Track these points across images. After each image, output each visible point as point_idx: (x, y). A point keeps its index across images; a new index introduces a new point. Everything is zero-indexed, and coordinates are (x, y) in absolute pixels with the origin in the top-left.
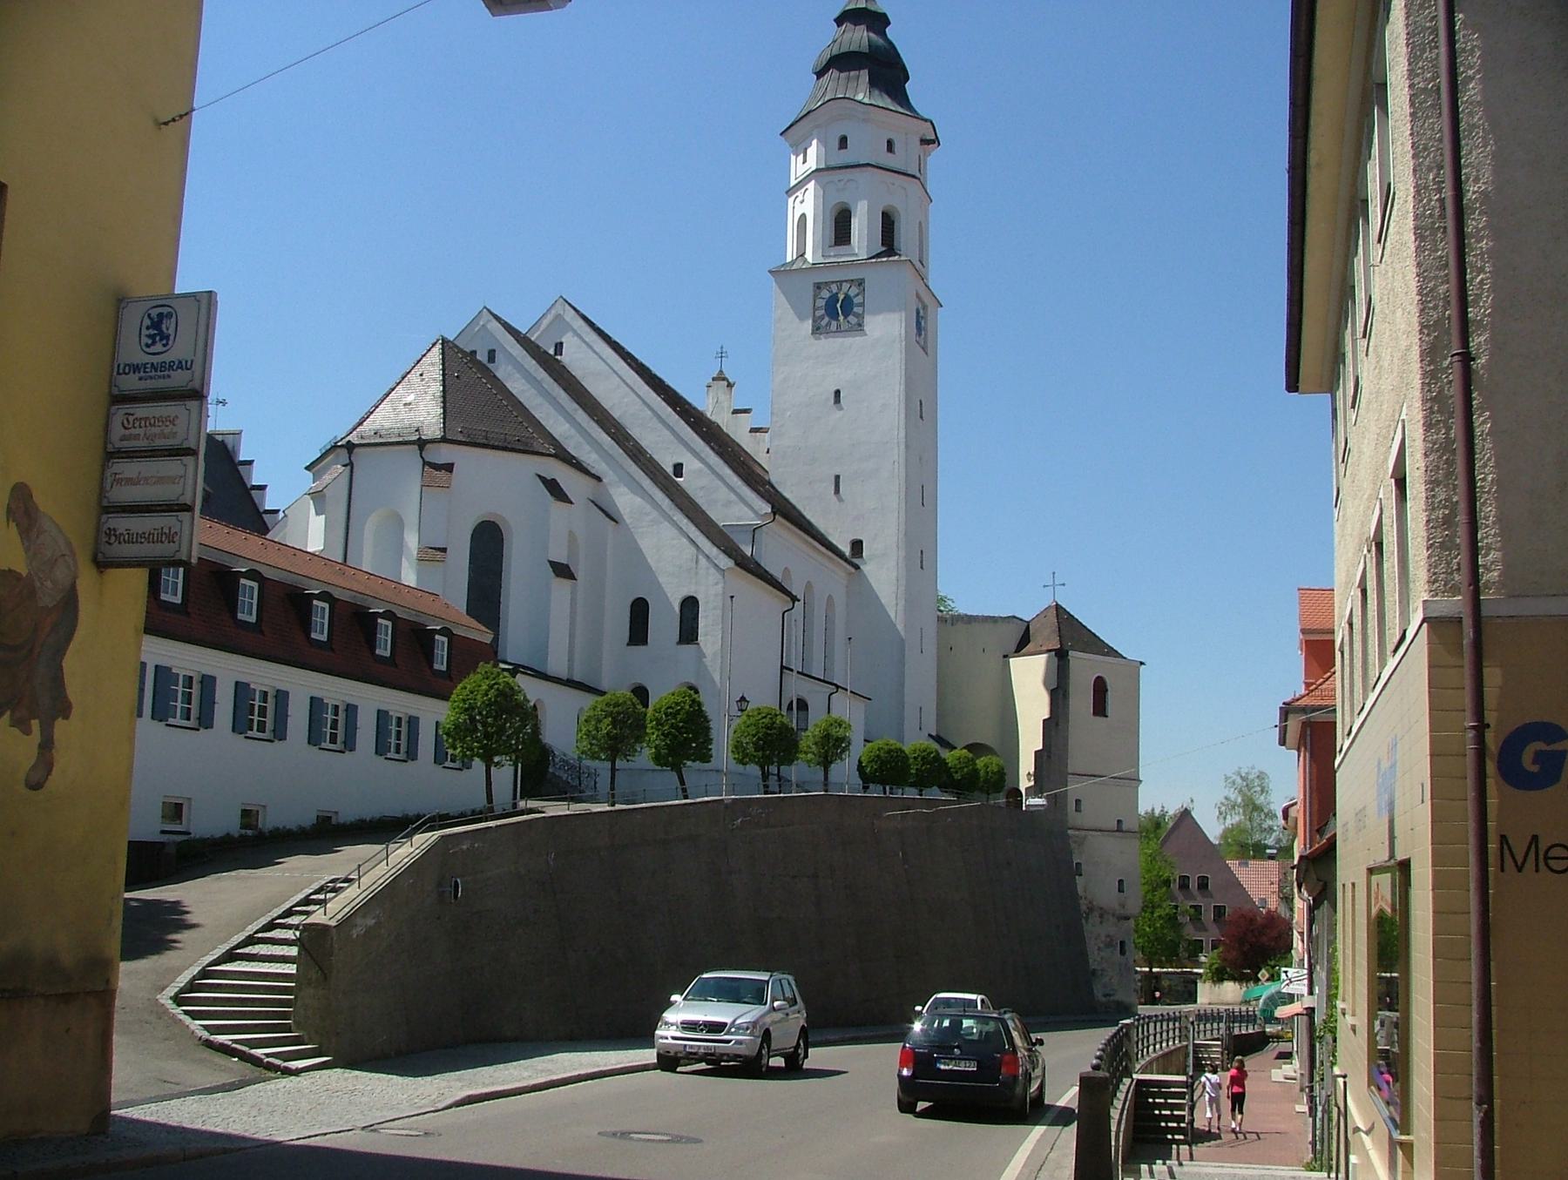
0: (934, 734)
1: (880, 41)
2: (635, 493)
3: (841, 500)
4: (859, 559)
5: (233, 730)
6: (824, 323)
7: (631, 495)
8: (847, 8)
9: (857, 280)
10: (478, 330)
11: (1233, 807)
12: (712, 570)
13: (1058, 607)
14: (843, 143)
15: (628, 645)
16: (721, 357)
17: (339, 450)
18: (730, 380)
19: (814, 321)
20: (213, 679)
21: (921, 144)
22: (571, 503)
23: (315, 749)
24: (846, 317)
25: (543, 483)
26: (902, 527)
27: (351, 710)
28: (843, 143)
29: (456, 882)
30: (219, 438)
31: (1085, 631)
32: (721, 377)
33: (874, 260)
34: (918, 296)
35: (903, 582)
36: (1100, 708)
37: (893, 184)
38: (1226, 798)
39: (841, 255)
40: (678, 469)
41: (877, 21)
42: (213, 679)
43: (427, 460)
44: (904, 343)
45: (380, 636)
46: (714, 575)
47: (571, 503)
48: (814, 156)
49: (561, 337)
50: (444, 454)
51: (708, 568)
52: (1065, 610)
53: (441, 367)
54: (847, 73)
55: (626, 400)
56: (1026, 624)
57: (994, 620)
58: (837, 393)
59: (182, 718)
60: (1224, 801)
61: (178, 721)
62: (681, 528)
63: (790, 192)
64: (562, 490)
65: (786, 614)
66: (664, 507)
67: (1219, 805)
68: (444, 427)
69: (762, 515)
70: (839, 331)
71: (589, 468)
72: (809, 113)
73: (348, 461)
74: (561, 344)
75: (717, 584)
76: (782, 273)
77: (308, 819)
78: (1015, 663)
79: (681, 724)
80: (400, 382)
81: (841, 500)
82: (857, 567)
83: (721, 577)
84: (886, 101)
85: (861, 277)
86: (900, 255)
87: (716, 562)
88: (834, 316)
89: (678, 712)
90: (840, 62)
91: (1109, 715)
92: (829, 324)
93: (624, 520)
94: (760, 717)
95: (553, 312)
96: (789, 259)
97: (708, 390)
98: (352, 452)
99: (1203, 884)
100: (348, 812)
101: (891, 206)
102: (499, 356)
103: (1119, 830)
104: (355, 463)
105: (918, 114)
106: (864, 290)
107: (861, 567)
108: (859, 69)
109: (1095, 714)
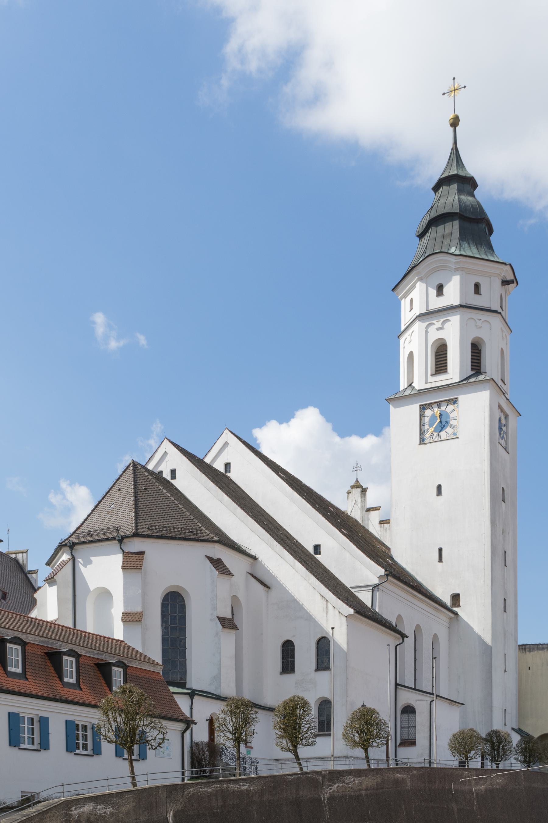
0: (516, 728)
8: (443, 176)
15: (281, 673)
16: (357, 470)
21: (502, 285)
23: (16, 750)
25: (208, 559)
30: (13, 556)
32: (357, 485)
34: (500, 407)
39: (441, 380)
40: (317, 548)
42: (47, 719)
53: (132, 483)
61: (26, 746)
65: (398, 647)
71: (247, 550)
96: (402, 388)
97: (348, 496)
101: (437, 285)
104: (75, 556)
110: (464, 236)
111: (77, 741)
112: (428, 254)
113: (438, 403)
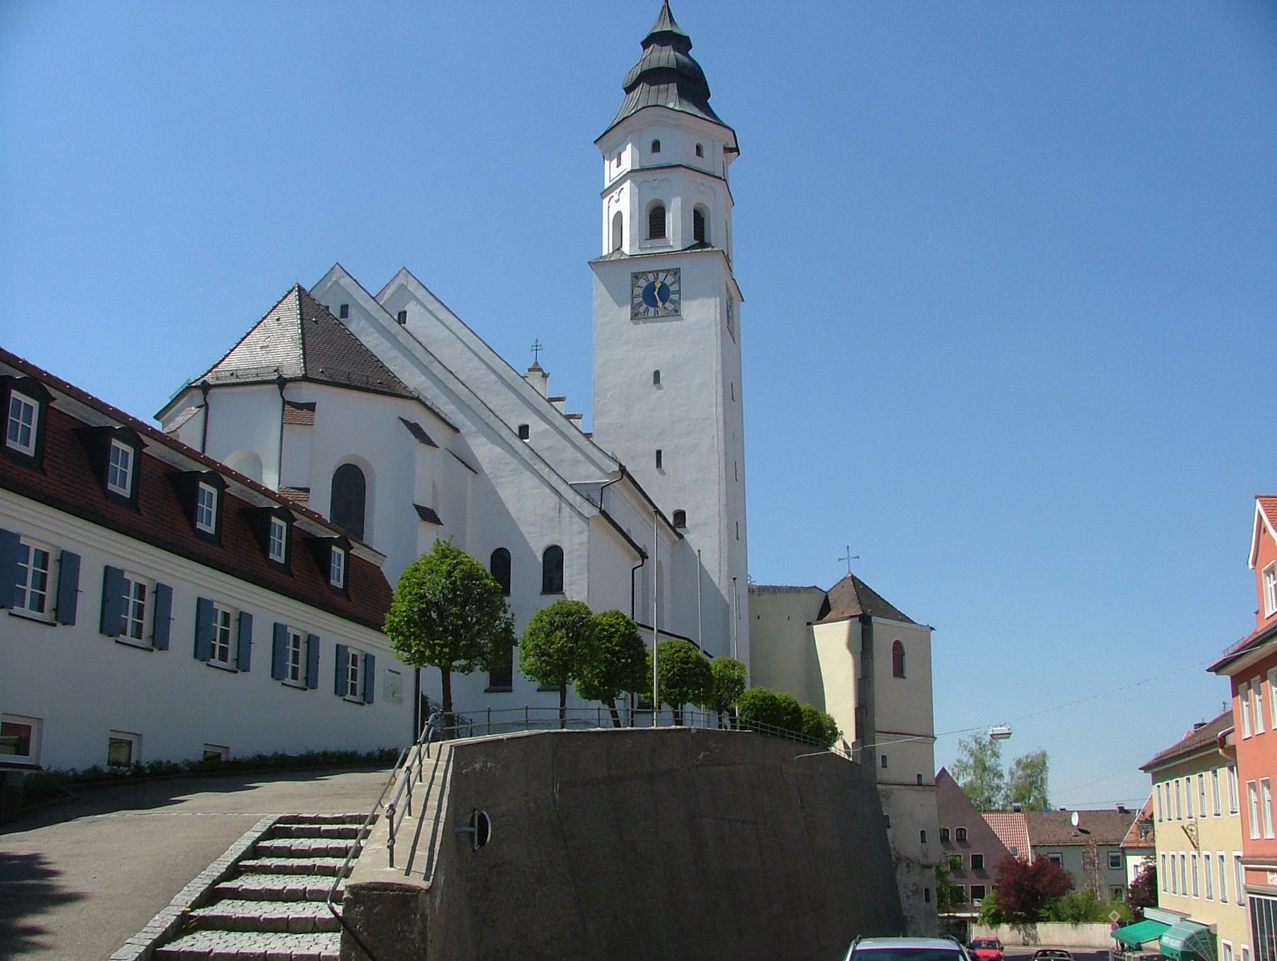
1: (686, 60)
2: (496, 444)
3: (663, 473)
4: (683, 529)
5: (102, 631)
6: (642, 309)
7: (490, 445)
8: (655, 31)
9: (672, 270)
10: (331, 286)
11: (965, 769)
12: (577, 519)
13: (853, 578)
14: (656, 146)
16: (537, 350)
17: (194, 392)
18: (545, 371)
19: (632, 308)
20: (76, 558)
22: (437, 447)
24: (664, 302)
26: (723, 498)
27: (245, 620)
28: (656, 146)
29: (482, 817)
31: (880, 601)
33: (689, 251)
35: (725, 549)
36: (899, 671)
37: (703, 184)
38: (959, 761)
39: (656, 247)
41: (682, 43)
42: (76, 558)
43: (287, 399)
44: (719, 327)
45: (274, 538)
46: (578, 524)
47: (437, 447)
48: (628, 159)
49: (404, 307)
50: (306, 393)
51: (571, 517)
52: (860, 581)
53: (298, 312)
54: (657, 86)
55: (471, 365)
56: (825, 594)
57: (797, 590)
58: (657, 374)
59: (31, 608)
60: (956, 763)
62: (543, 477)
63: (605, 193)
64: (425, 433)
65: (635, 570)
66: (524, 456)
67: (952, 767)
68: (305, 367)
69: (610, 474)
70: (656, 316)
72: (624, 119)
73: (203, 403)
74: (405, 313)
75: (581, 532)
76: (598, 264)
77: (196, 755)
78: (818, 629)
79: (617, 648)
80: (256, 327)
81: (663, 473)
82: (681, 536)
83: (585, 525)
84: (694, 110)
85: (677, 267)
86: (713, 247)
87: (579, 509)
88: (654, 304)
89: (611, 636)
90: (651, 76)
91: (907, 676)
92: (647, 310)
93: (484, 471)
94: (673, 651)
95: (397, 282)
98: (207, 394)
99: (961, 837)
100: (242, 748)
102: (352, 311)
103: (920, 784)
104: (209, 404)
105: (719, 120)
106: (680, 278)
107: (685, 536)
108: (668, 83)
109: (895, 675)
110: (683, 94)
111: (213, 642)
112: (642, 107)
113: (655, 274)
